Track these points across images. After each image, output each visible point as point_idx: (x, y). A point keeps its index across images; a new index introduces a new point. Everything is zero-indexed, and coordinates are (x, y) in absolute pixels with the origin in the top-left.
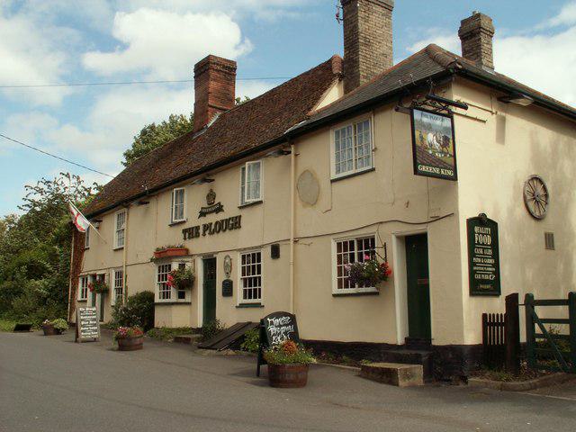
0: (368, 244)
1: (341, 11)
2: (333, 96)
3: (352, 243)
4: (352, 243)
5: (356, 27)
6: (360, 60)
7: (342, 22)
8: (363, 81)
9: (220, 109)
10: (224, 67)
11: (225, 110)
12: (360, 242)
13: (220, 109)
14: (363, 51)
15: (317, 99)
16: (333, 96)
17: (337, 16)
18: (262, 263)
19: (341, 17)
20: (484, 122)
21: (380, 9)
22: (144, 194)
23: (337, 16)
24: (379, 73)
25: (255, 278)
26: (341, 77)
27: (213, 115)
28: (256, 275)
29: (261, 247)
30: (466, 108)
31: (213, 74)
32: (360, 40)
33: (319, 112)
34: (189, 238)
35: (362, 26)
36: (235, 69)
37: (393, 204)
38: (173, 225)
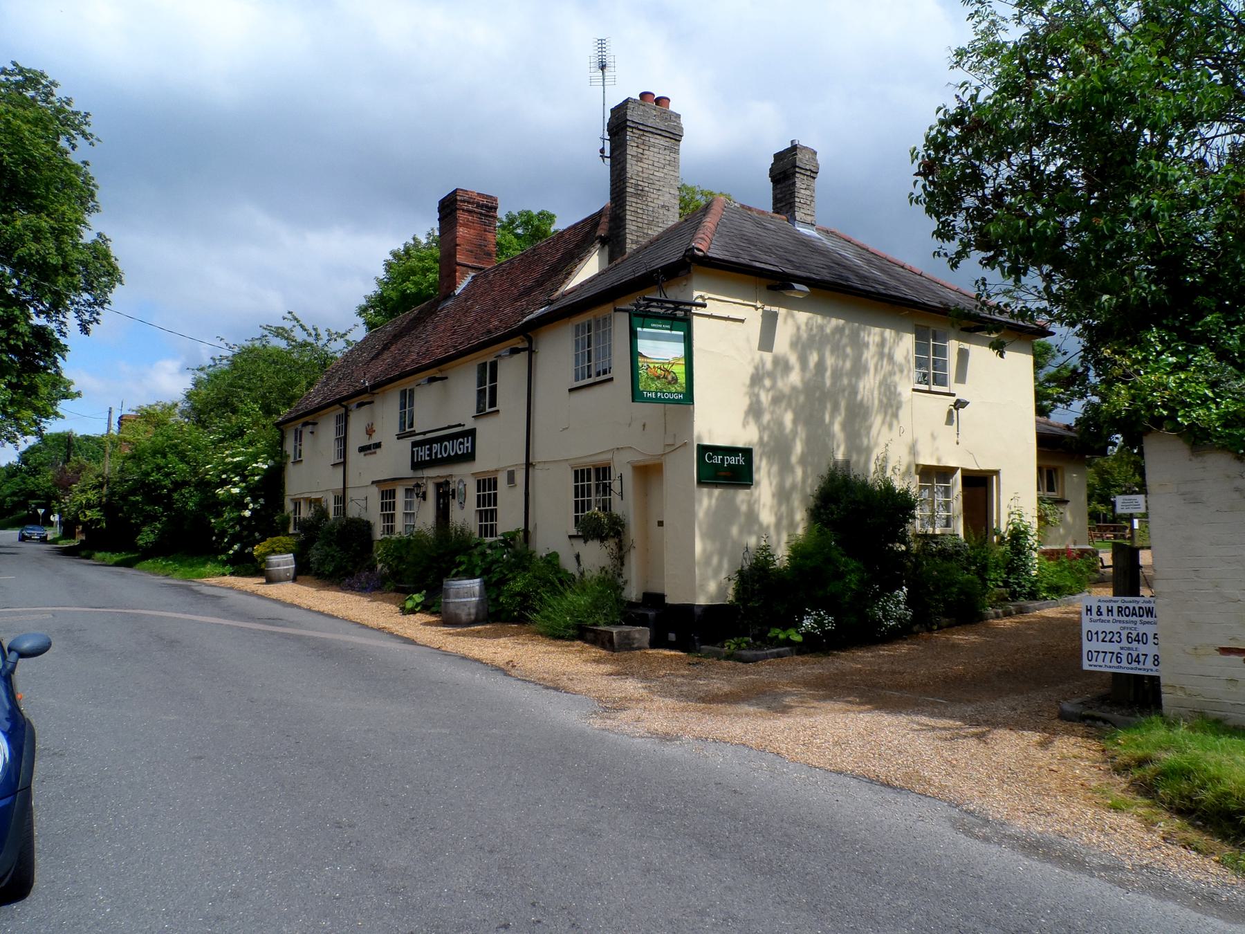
0: (603, 472)
1: (608, 144)
2: (590, 267)
3: (589, 471)
4: (589, 471)
5: (624, 169)
6: (628, 217)
7: (608, 161)
8: (630, 247)
9: (473, 268)
10: (479, 205)
11: (481, 269)
12: (597, 470)
13: (473, 268)
14: (632, 204)
15: (569, 274)
16: (590, 267)
17: (602, 151)
18: (499, 492)
19: (607, 153)
20: (742, 321)
21: (662, 141)
22: (364, 391)
23: (602, 151)
24: (656, 234)
25: (492, 510)
26: (604, 241)
27: (463, 276)
28: (492, 507)
29: (497, 471)
30: (704, 306)
31: (462, 216)
32: (628, 190)
33: (564, 295)
34: (1147, 518)
35: (632, 168)
36: (496, 208)
37: (630, 425)
38: (400, 437)
